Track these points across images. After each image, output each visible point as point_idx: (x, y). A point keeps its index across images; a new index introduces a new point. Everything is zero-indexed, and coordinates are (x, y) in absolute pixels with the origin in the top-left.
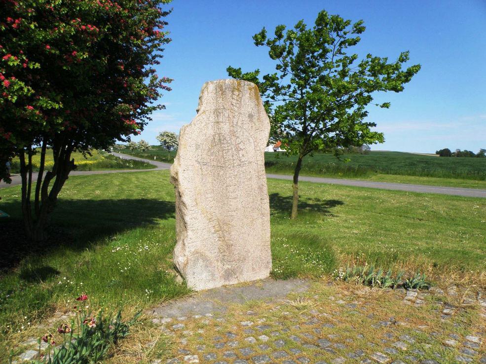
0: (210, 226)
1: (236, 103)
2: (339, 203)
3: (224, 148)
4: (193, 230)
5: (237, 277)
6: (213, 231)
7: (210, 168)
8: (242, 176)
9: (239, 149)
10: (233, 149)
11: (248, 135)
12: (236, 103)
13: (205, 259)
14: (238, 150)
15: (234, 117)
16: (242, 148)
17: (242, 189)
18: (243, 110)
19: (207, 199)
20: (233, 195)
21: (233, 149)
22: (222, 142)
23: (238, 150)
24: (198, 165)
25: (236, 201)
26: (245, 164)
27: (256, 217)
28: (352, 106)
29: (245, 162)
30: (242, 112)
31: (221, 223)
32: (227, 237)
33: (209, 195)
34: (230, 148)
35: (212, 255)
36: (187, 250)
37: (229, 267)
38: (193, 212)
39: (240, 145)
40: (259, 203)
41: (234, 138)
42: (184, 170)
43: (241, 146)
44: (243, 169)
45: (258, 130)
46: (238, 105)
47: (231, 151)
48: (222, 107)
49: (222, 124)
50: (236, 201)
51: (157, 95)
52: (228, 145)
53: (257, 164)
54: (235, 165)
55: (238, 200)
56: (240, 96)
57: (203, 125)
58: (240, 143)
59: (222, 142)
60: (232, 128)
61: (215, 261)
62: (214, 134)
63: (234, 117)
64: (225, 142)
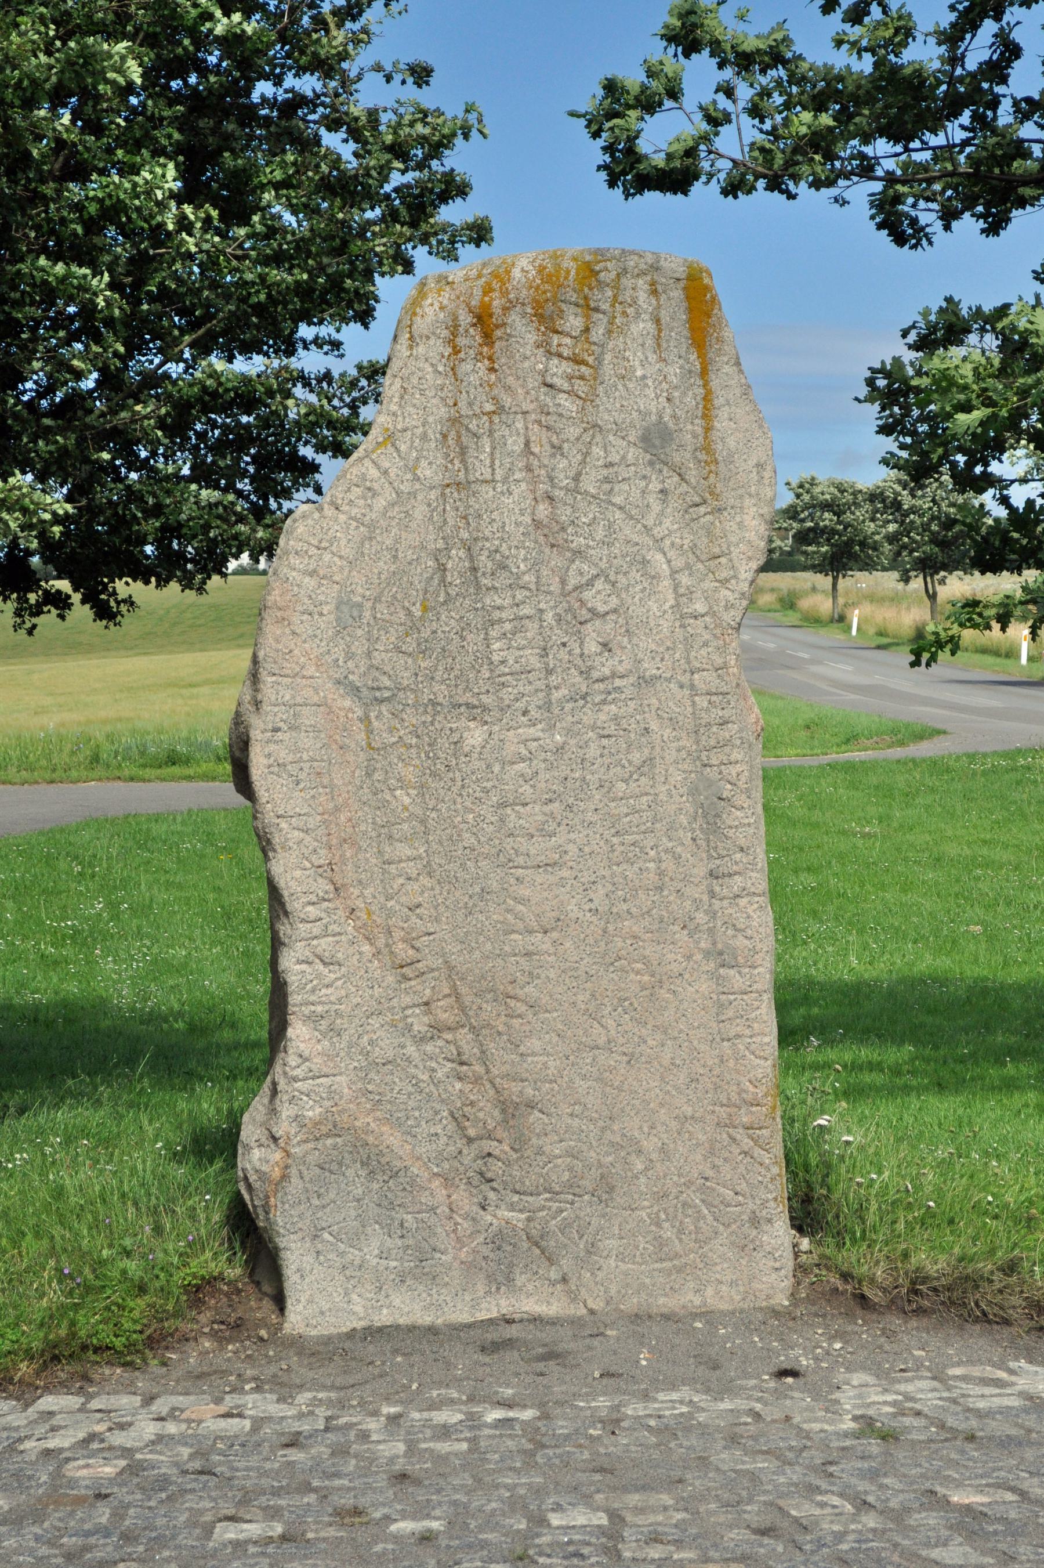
0: (407, 1000)
1: (570, 378)
2: (945, 732)
3: (496, 615)
4: (313, 1019)
5: (564, 1280)
6: (420, 1024)
7: (411, 718)
8: (593, 751)
9: (584, 614)
10: (549, 616)
11: (635, 538)
12: (570, 378)
13: (376, 1164)
14: (577, 618)
15: (557, 449)
16: (602, 608)
17: (590, 816)
18: (607, 412)
19: (393, 869)
20: (537, 848)
21: (549, 616)
22: (486, 581)
23: (577, 618)
24: (347, 703)
25: (553, 879)
26: (617, 689)
27: (675, 968)
28: (396, 190)
29: (618, 682)
30: (604, 418)
31: (463, 990)
32: (502, 1059)
33: (404, 850)
34: (526, 610)
35: (417, 1145)
36: (286, 1111)
37: (518, 1218)
38: (316, 929)
39: (587, 595)
40: (698, 892)
41: (557, 560)
42: (276, 730)
43: (597, 597)
44: (603, 717)
45: (702, 510)
46: (581, 388)
47: (532, 627)
48: (489, 407)
49: (487, 492)
50: (553, 879)
51: (510, 1280)
52: (520, 595)
53: (692, 686)
54: (556, 695)
55: (565, 873)
56: (598, 333)
57: (380, 503)
58: (590, 583)
59: (486, 581)
60: (543, 510)
61: (436, 1183)
62: (441, 544)
63: (557, 449)
64: (502, 580)
